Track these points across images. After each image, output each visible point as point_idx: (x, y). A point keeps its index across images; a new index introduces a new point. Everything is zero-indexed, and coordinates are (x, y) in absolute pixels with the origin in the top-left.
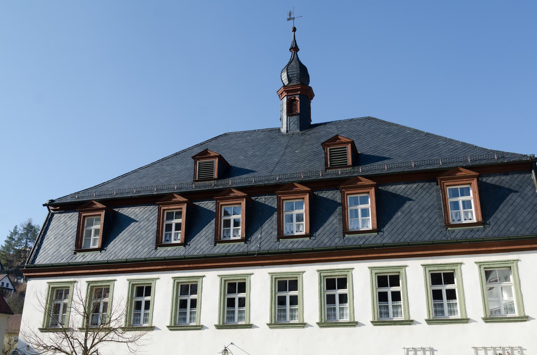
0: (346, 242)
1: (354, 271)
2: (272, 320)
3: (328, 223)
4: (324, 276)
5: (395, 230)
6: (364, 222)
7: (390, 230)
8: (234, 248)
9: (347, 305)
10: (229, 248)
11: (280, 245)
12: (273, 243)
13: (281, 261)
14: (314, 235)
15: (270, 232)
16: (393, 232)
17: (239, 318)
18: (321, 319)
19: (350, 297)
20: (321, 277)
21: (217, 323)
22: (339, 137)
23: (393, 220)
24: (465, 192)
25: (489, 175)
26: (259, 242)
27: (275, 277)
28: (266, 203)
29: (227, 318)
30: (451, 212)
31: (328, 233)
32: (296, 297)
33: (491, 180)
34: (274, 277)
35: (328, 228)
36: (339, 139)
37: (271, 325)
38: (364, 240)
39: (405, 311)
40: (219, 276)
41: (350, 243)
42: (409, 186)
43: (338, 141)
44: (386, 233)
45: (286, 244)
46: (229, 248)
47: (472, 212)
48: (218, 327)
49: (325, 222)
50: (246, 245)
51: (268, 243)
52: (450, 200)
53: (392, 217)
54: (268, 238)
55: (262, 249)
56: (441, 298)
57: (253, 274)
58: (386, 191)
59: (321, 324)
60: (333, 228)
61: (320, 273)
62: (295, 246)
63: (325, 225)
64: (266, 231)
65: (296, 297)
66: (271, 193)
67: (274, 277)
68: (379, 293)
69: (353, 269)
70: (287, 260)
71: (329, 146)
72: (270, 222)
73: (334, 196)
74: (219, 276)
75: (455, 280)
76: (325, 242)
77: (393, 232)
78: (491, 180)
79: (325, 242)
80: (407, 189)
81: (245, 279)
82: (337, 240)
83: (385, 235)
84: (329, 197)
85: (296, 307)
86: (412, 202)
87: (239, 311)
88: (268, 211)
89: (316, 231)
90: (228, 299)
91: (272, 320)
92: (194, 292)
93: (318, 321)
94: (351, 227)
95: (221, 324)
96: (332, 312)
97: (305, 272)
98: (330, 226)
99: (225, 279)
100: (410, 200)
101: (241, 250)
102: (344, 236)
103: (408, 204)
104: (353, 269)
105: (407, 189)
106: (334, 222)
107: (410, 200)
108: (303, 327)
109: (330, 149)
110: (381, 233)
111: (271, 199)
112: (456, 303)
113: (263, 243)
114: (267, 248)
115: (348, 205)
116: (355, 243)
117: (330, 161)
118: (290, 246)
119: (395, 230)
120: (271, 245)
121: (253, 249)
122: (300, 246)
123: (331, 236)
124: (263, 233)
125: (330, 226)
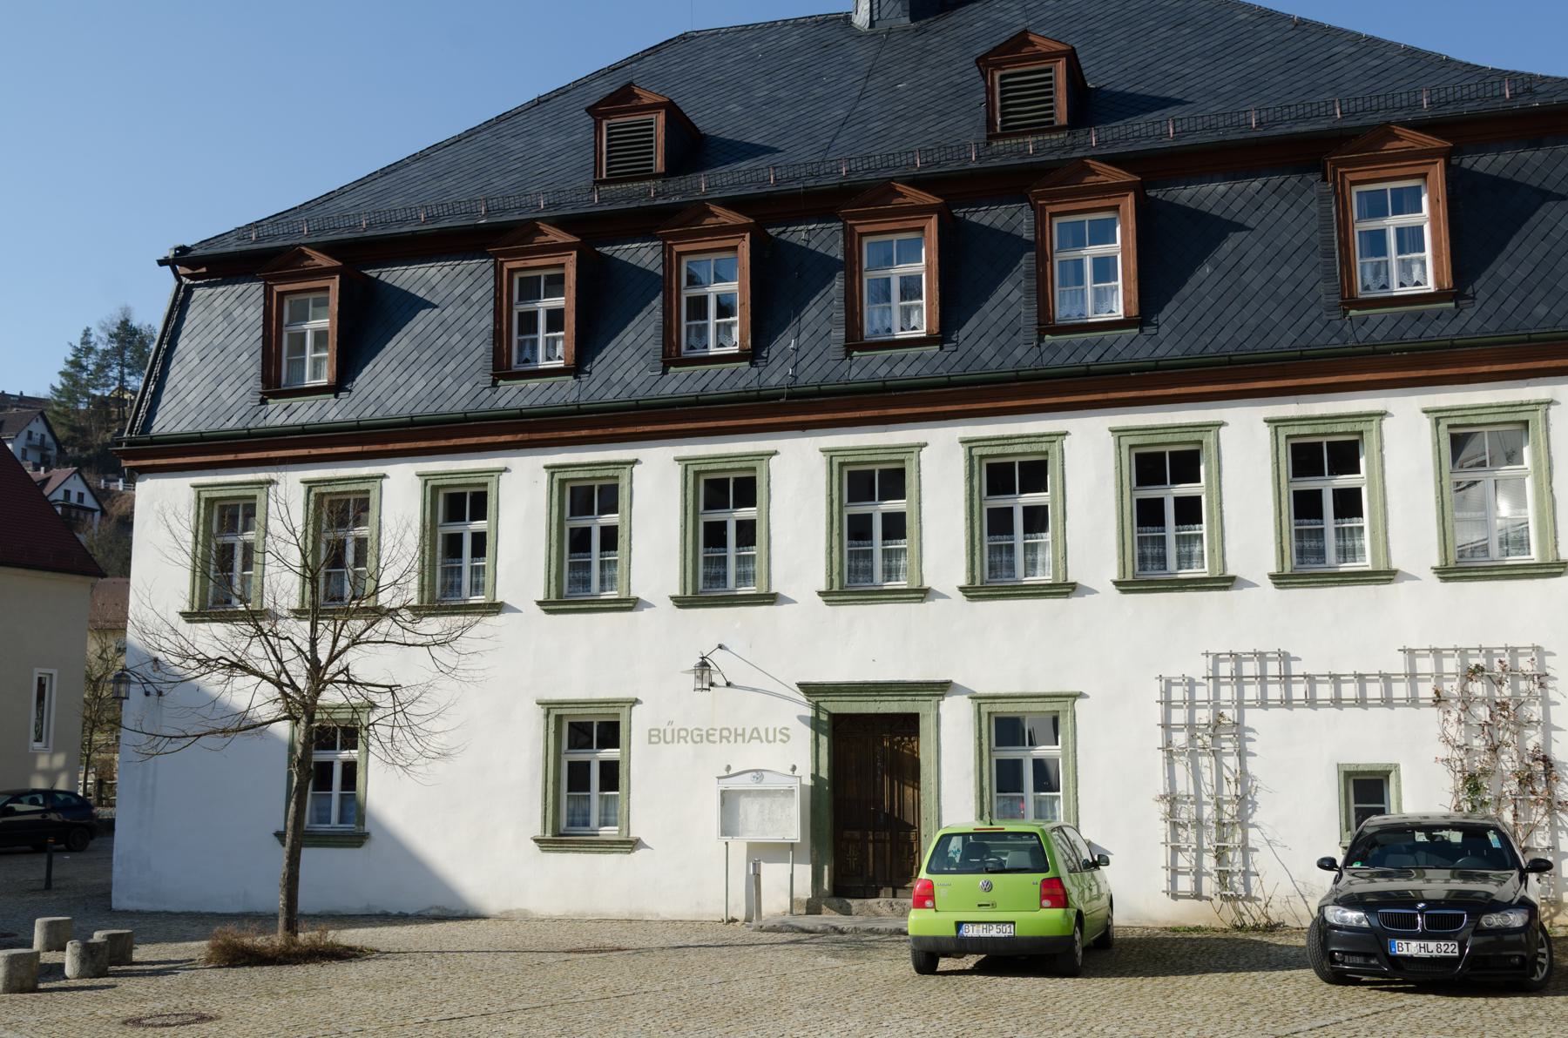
0: (1047, 356)
1: (1387, 422)
2: (832, 581)
3: (993, 300)
4: (981, 457)
5: (1193, 318)
6: (1100, 296)
7: (1176, 318)
8: (720, 379)
9: (1047, 537)
10: (706, 380)
11: (855, 370)
12: (834, 364)
13: (857, 414)
14: (954, 338)
15: (822, 331)
16: (1186, 325)
17: (738, 577)
18: (973, 578)
19: (1054, 516)
20: (971, 458)
21: (677, 592)
22: (1031, 38)
23: (1186, 290)
24: (1405, 202)
25: (977, 201)
26: (792, 361)
27: (841, 460)
28: (812, 246)
29: (705, 577)
30: (1362, 266)
31: (993, 332)
32: (901, 517)
33: (1486, 163)
34: (836, 461)
35: (994, 317)
36: (1032, 44)
37: (829, 596)
38: (1098, 351)
39: (1212, 551)
40: (678, 460)
41: (1058, 361)
42: (1239, 186)
43: (1027, 50)
44: (1165, 329)
45: (872, 367)
46: (706, 380)
47: (1423, 263)
48: (682, 602)
49: (987, 300)
50: (755, 371)
51: (817, 364)
52: (1362, 226)
53: (1183, 282)
54: (819, 348)
55: (802, 380)
56: (1318, 514)
57: (776, 453)
58: (1170, 204)
59: (972, 592)
60: (1010, 316)
61: (970, 449)
62: (897, 372)
63: (987, 307)
64: (813, 327)
65: (901, 517)
66: (826, 216)
67: (836, 461)
68: (1139, 501)
69: (1065, 434)
70: (875, 413)
71: (998, 67)
72: (824, 303)
73: (1014, 222)
74: (678, 460)
75: (1363, 462)
76: (985, 357)
77: (1186, 325)
78: (1486, 163)
79: (985, 357)
80: (1232, 195)
81: (754, 469)
82: (1019, 352)
83: (1161, 336)
84: (998, 224)
85: (1193, 530)
86: (1244, 234)
87: (738, 557)
88: (818, 270)
89: (960, 325)
90: (706, 524)
91: (832, 581)
92: (611, 505)
93: (963, 582)
94: (1063, 311)
95: (689, 593)
96: (1005, 558)
97: (926, 445)
98: (1000, 310)
99: (697, 468)
100: (1240, 227)
101: (741, 384)
102: (1041, 340)
103: (1233, 240)
104: (1065, 434)
105: (1232, 195)
106: (1012, 298)
107: (1240, 227)
108: (922, 600)
109: (1002, 77)
110: (1150, 330)
111: (824, 235)
112: (1201, 536)
113: (803, 364)
114: (817, 379)
115: (1056, 247)
116: (1072, 360)
117: (1002, 115)
118: (882, 372)
119: (1193, 318)
120: (827, 369)
121: (774, 381)
122: (912, 372)
123: (1003, 339)
124: (804, 336)
125: (1000, 310)
